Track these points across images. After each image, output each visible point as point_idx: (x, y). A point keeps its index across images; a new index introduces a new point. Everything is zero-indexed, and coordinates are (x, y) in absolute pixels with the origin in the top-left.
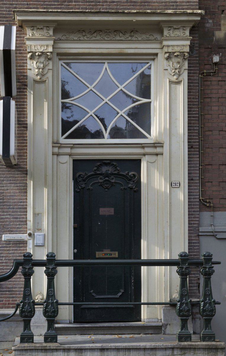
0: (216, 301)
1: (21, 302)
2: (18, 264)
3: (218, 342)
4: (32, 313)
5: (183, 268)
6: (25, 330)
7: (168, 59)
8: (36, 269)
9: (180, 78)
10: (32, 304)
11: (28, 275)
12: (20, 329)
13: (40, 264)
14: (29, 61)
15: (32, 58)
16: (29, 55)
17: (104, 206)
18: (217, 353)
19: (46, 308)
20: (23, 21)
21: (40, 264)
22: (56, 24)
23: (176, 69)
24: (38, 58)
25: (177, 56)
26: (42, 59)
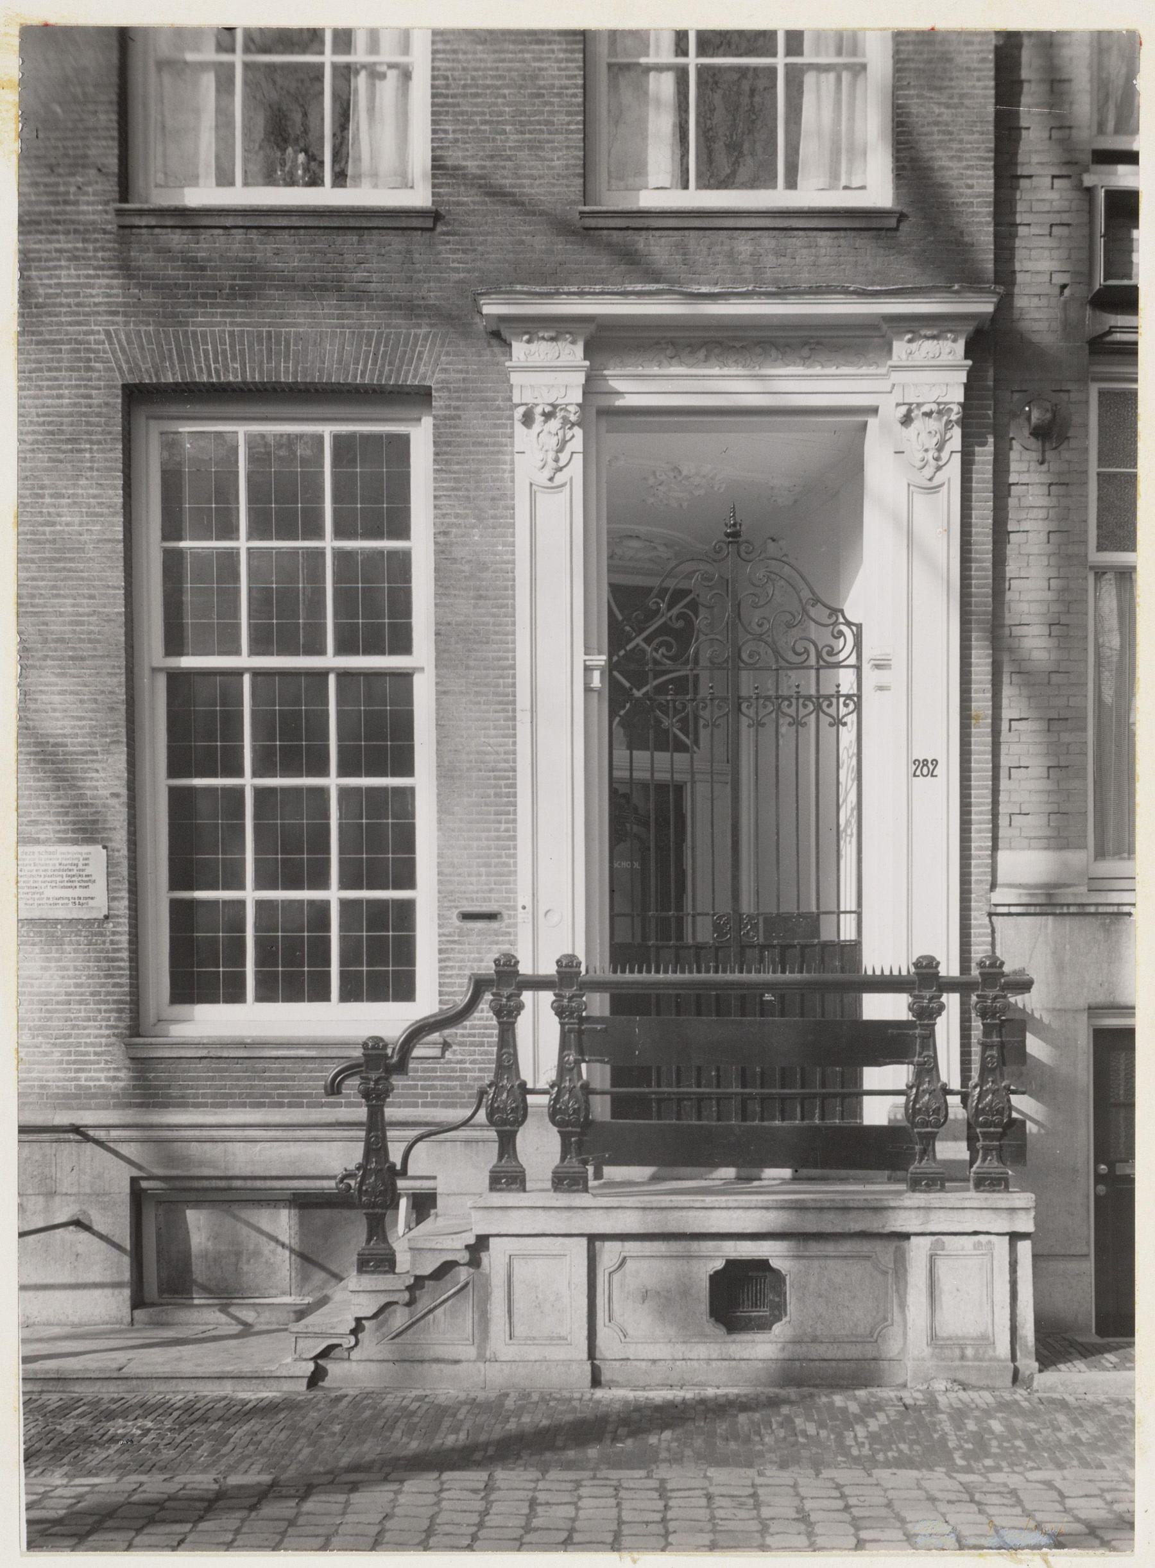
0: (1006, 969)
1: (490, 1086)
2: (480, 985)
3: (989, 513)
4: (521, 1113)
5: (923, 998)
6: (501, 1156)
7: (907, 420)
8: (527, 996)
9: (940, 477)
10: (517, 1092)
11: (507, 1015)
12: (490, 1155)
13: (538, 984)
14: (519, 428)
15: (528, 419)
16: (519, 412)
17: (877, 1061)
18: (139, 269)
19: (556, 1100)
20: (503, 319)
21: (538, 984)
22: (592, 327)
23: (926, 450)
24: (545, 422)
25: (928, 415)
26: (554, 424)
